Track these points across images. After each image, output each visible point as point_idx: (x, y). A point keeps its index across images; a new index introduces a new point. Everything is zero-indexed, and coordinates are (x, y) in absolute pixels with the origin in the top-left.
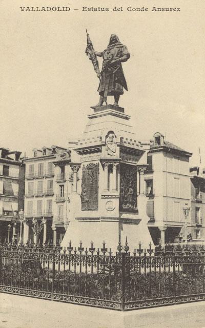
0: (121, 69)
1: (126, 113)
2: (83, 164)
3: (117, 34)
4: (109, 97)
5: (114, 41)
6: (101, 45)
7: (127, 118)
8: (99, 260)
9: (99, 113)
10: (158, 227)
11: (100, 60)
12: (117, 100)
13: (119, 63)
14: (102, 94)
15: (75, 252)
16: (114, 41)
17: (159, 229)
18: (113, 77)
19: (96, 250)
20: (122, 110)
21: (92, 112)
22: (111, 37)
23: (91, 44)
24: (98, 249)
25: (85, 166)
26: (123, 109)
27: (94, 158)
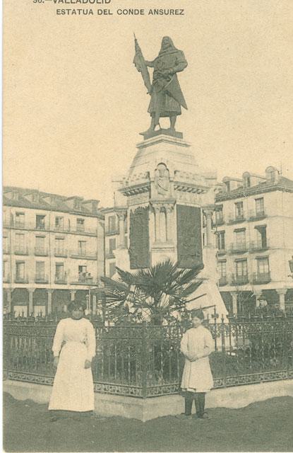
0: (176, 82)
1: (186, 138)
2: (130, 208)
3: (168, 35)
4: (161, 119)
5: (167, 44)
6: (151, 53)
7: (186, 145)
8: (105, 417)
9: (150, 140)
10: (275, 290)
11: (151, 70)
12: (173, 123)
13: (174, 74)
14: (153, 114)
15: (223, 320)
16: (167, 44)
17: (276, 292)
18: (164, 80)
19: (220, 317)
20: (180, 135)
21: (141, 139)
22: (163, 41)
23: (140, 51)
24: (223, 315)
25: (133, 211)
26: (181, 133)
27: (143, 200)
